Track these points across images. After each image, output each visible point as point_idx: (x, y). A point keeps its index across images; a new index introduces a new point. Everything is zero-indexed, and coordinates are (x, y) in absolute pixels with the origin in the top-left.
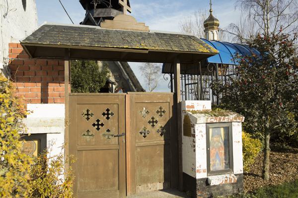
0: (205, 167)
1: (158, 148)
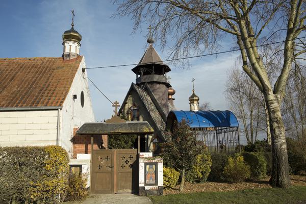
0: (143, 181)
1: (129, 174)
